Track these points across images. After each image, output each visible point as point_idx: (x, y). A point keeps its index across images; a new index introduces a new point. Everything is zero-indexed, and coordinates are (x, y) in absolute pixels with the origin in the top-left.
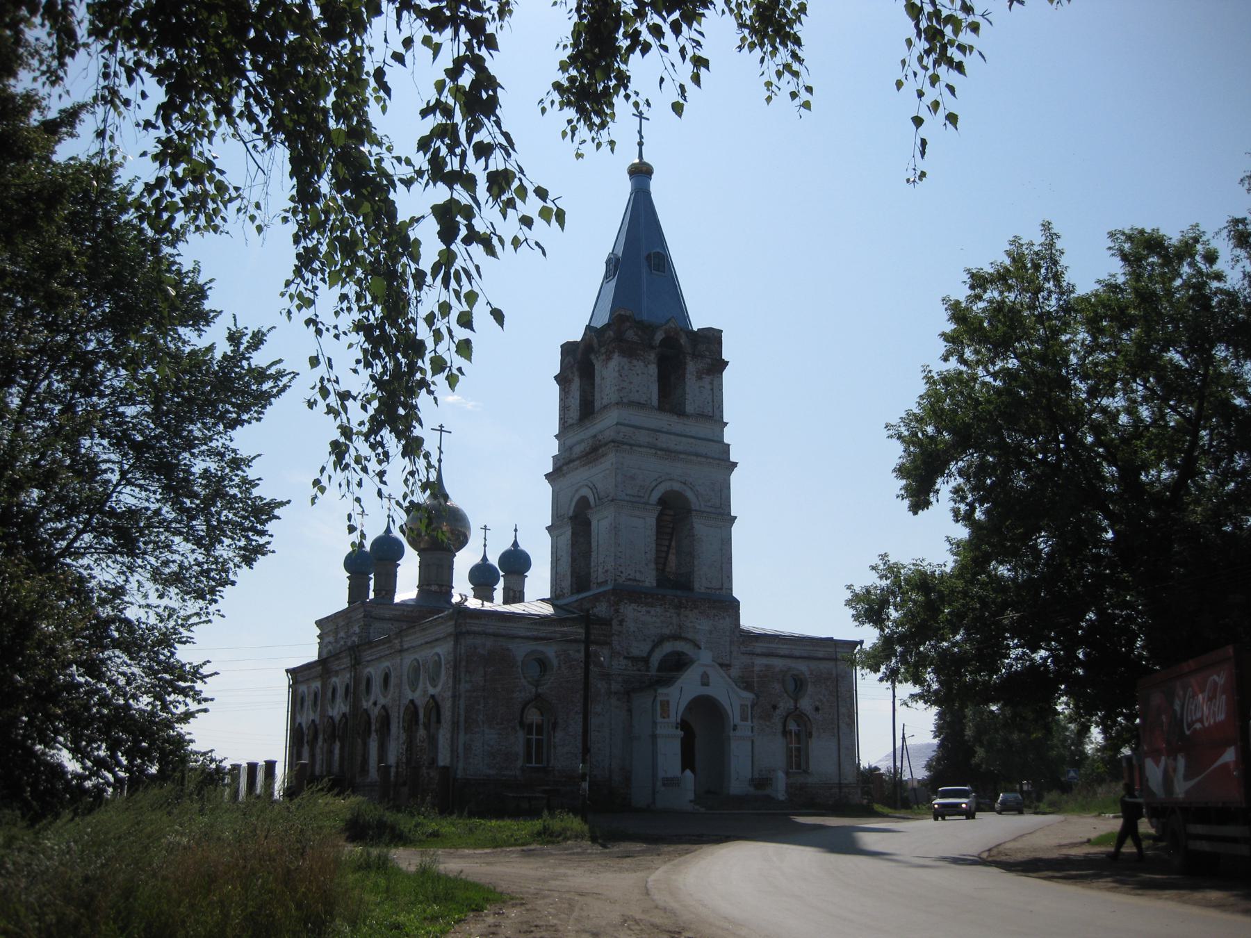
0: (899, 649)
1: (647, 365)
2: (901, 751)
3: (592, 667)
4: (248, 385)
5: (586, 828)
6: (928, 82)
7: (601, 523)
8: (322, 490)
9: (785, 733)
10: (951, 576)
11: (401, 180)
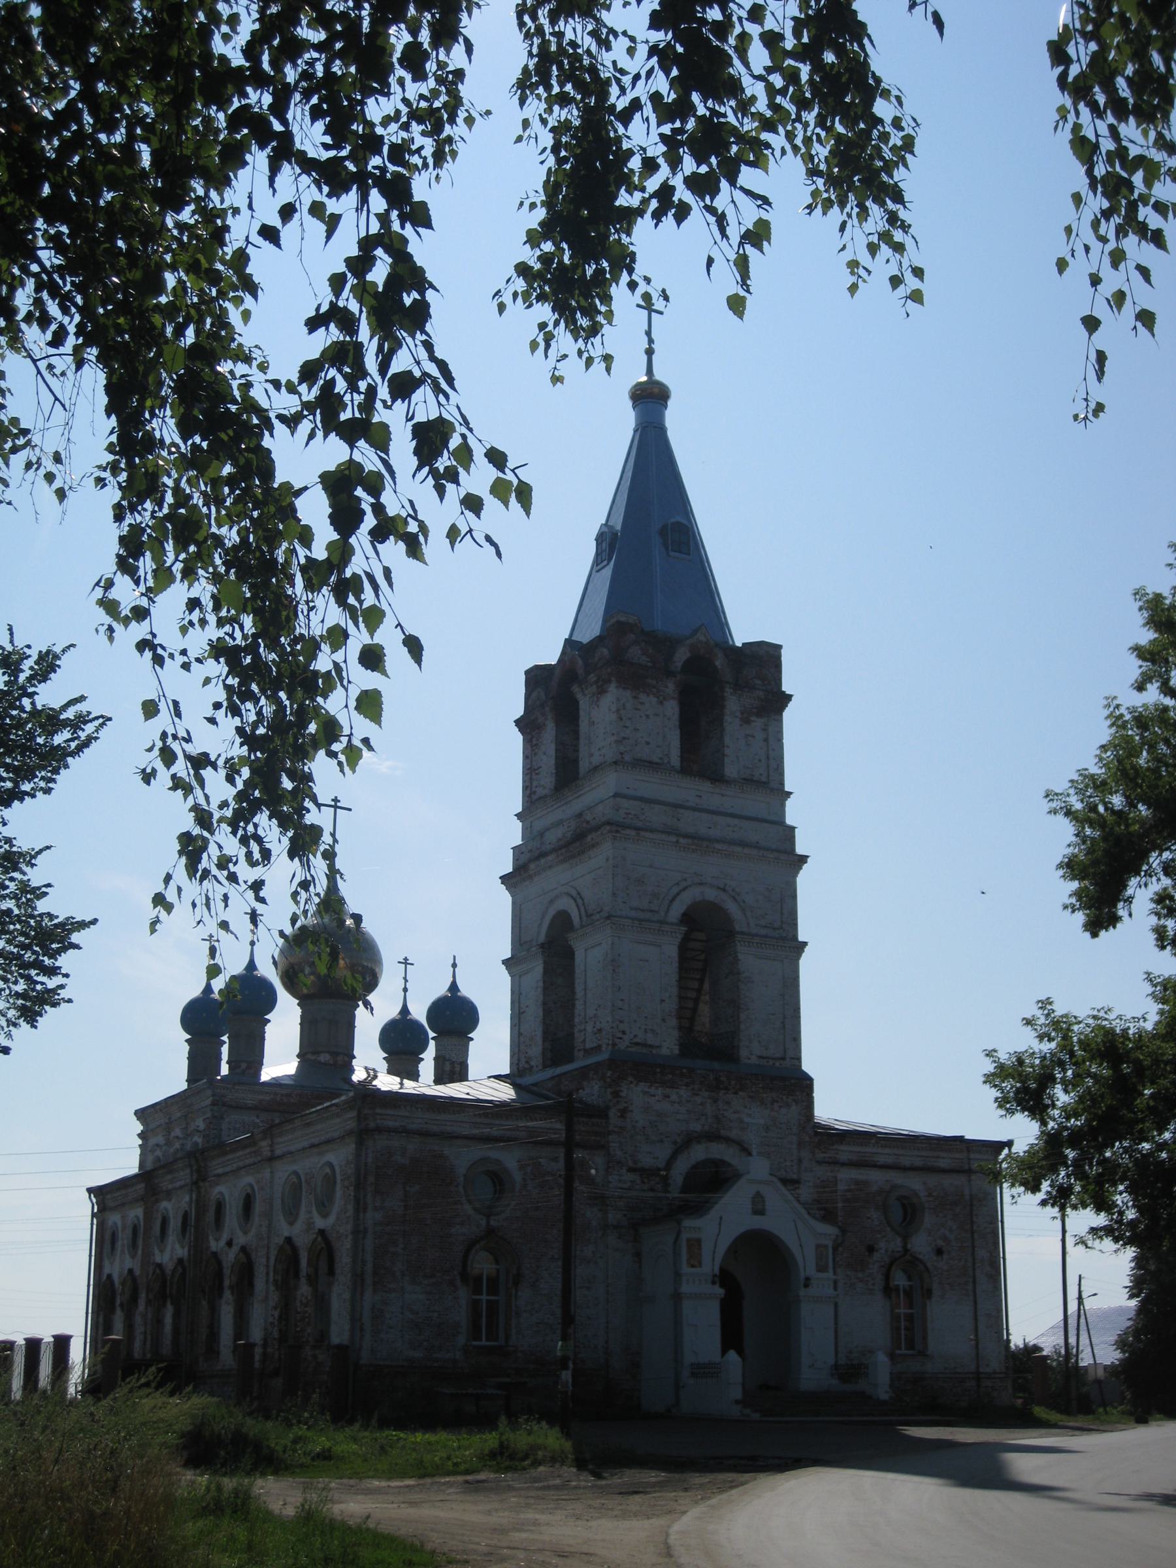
0: (1071, 1154)
1: (662, 706)
2: (1075, 1320)
3: (576, 1184)
4: (31, 736)
5: (568, 1445)
6: (1107, 260)
7: (591, 954)
8: (169, 908)
9: (888, 1290)
10: (1154, 1036)
11: (281, 417)
